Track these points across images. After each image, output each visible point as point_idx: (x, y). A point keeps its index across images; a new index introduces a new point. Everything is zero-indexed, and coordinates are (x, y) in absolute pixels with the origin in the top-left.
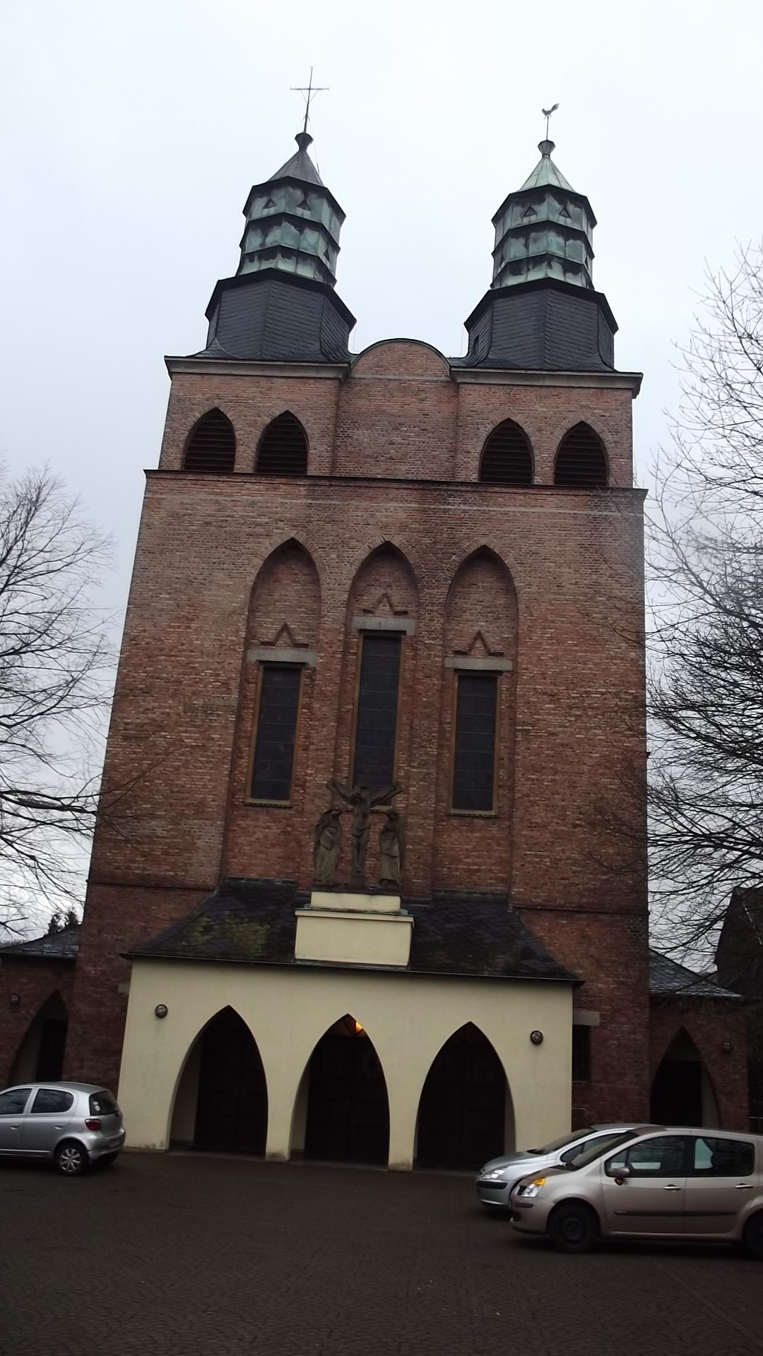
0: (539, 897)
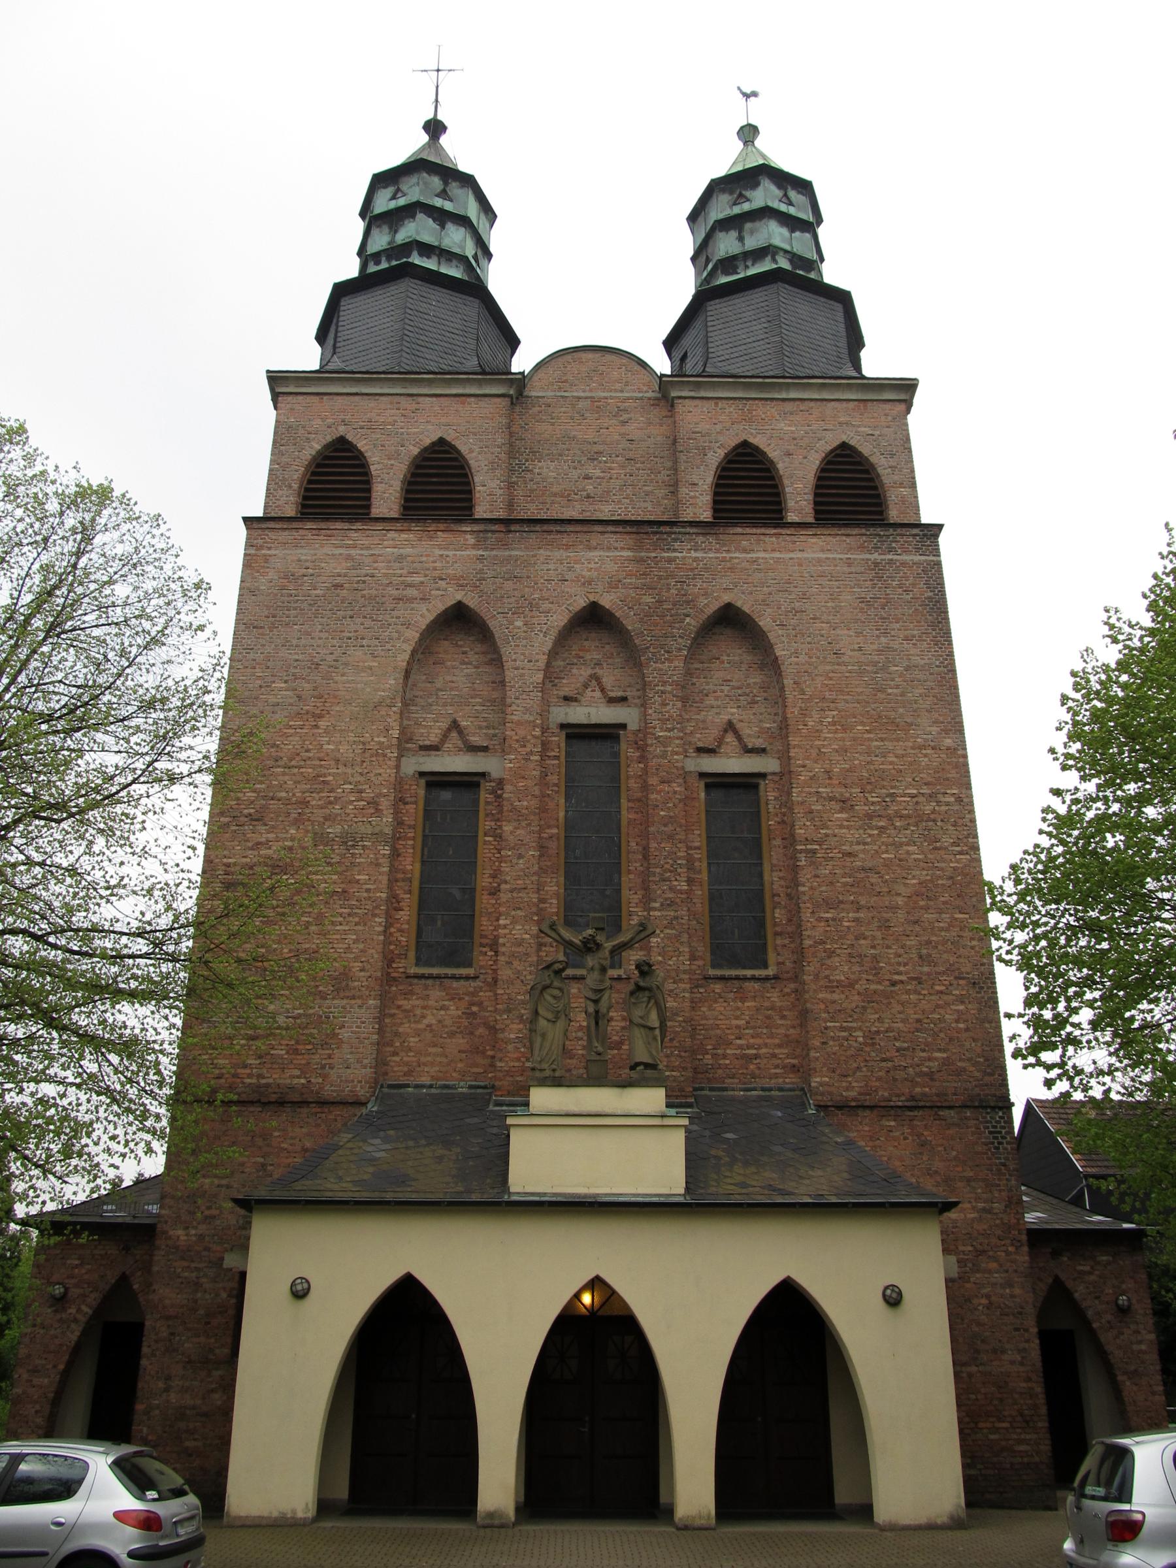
0: (852, 1089)
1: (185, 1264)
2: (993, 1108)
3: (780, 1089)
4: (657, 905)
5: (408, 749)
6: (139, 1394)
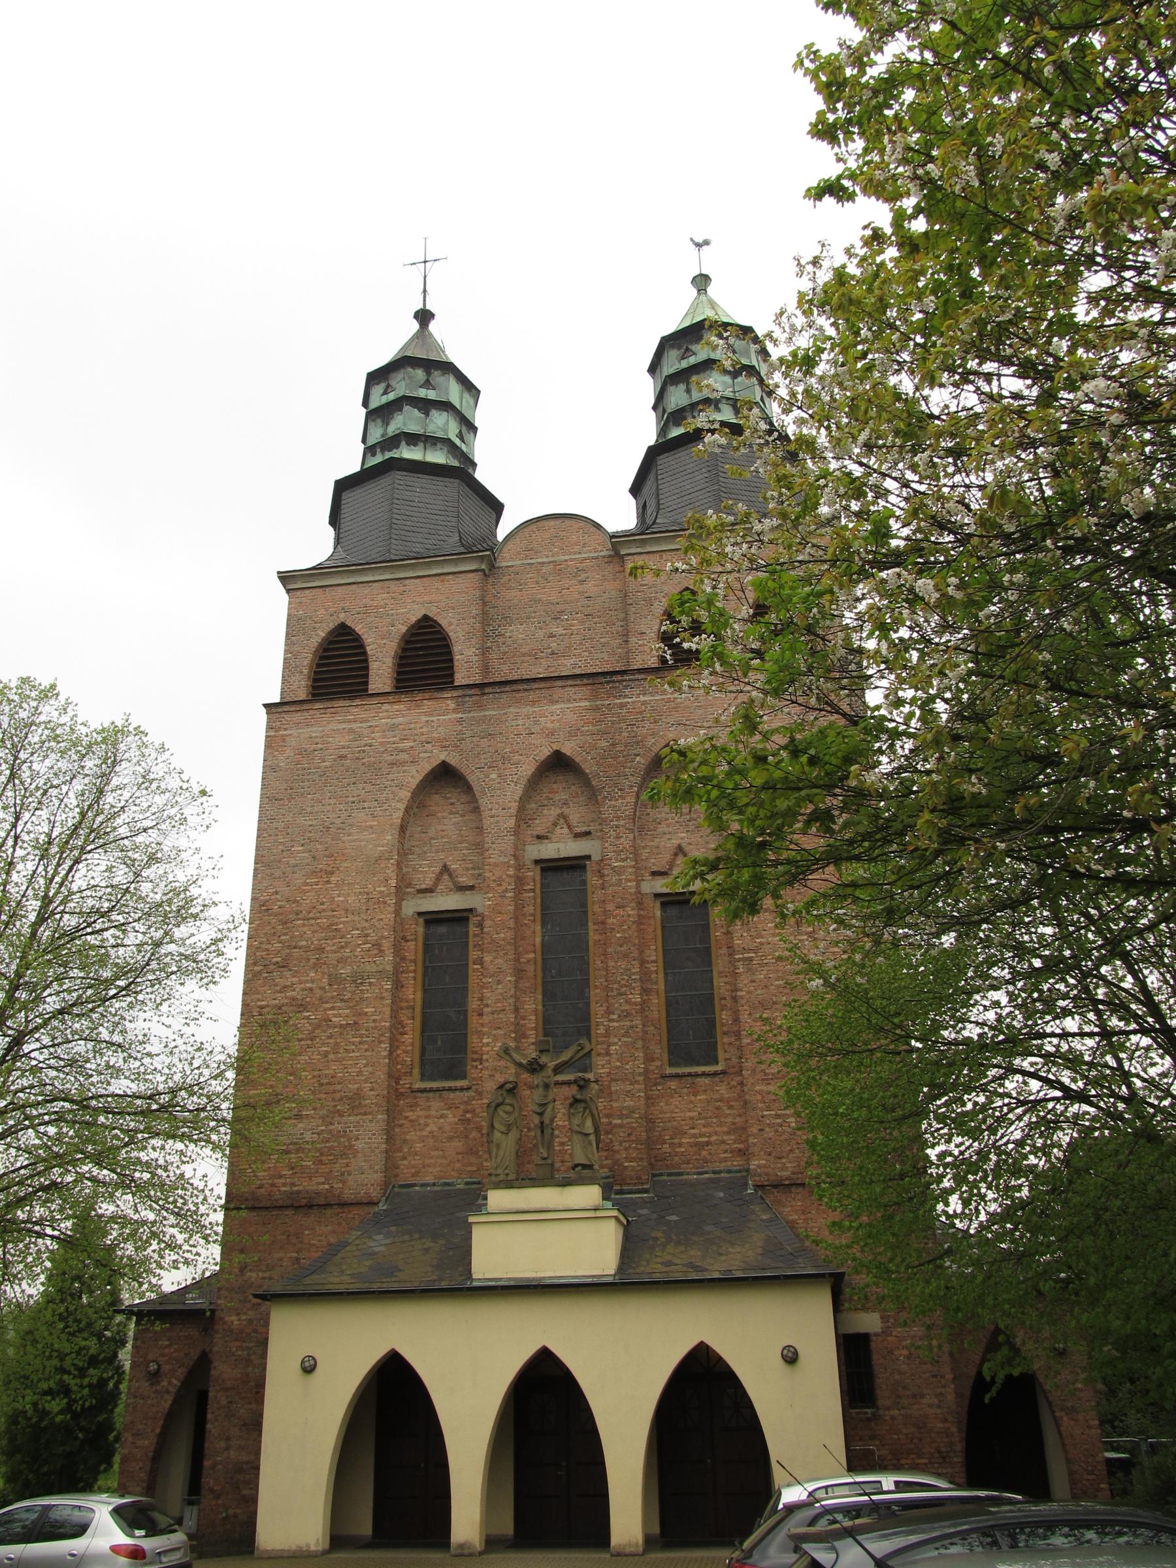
1: (238, 1344)
3: (729, 1171)
4: (615, 1017)
5: (408, 893)
6: (206, 1452)
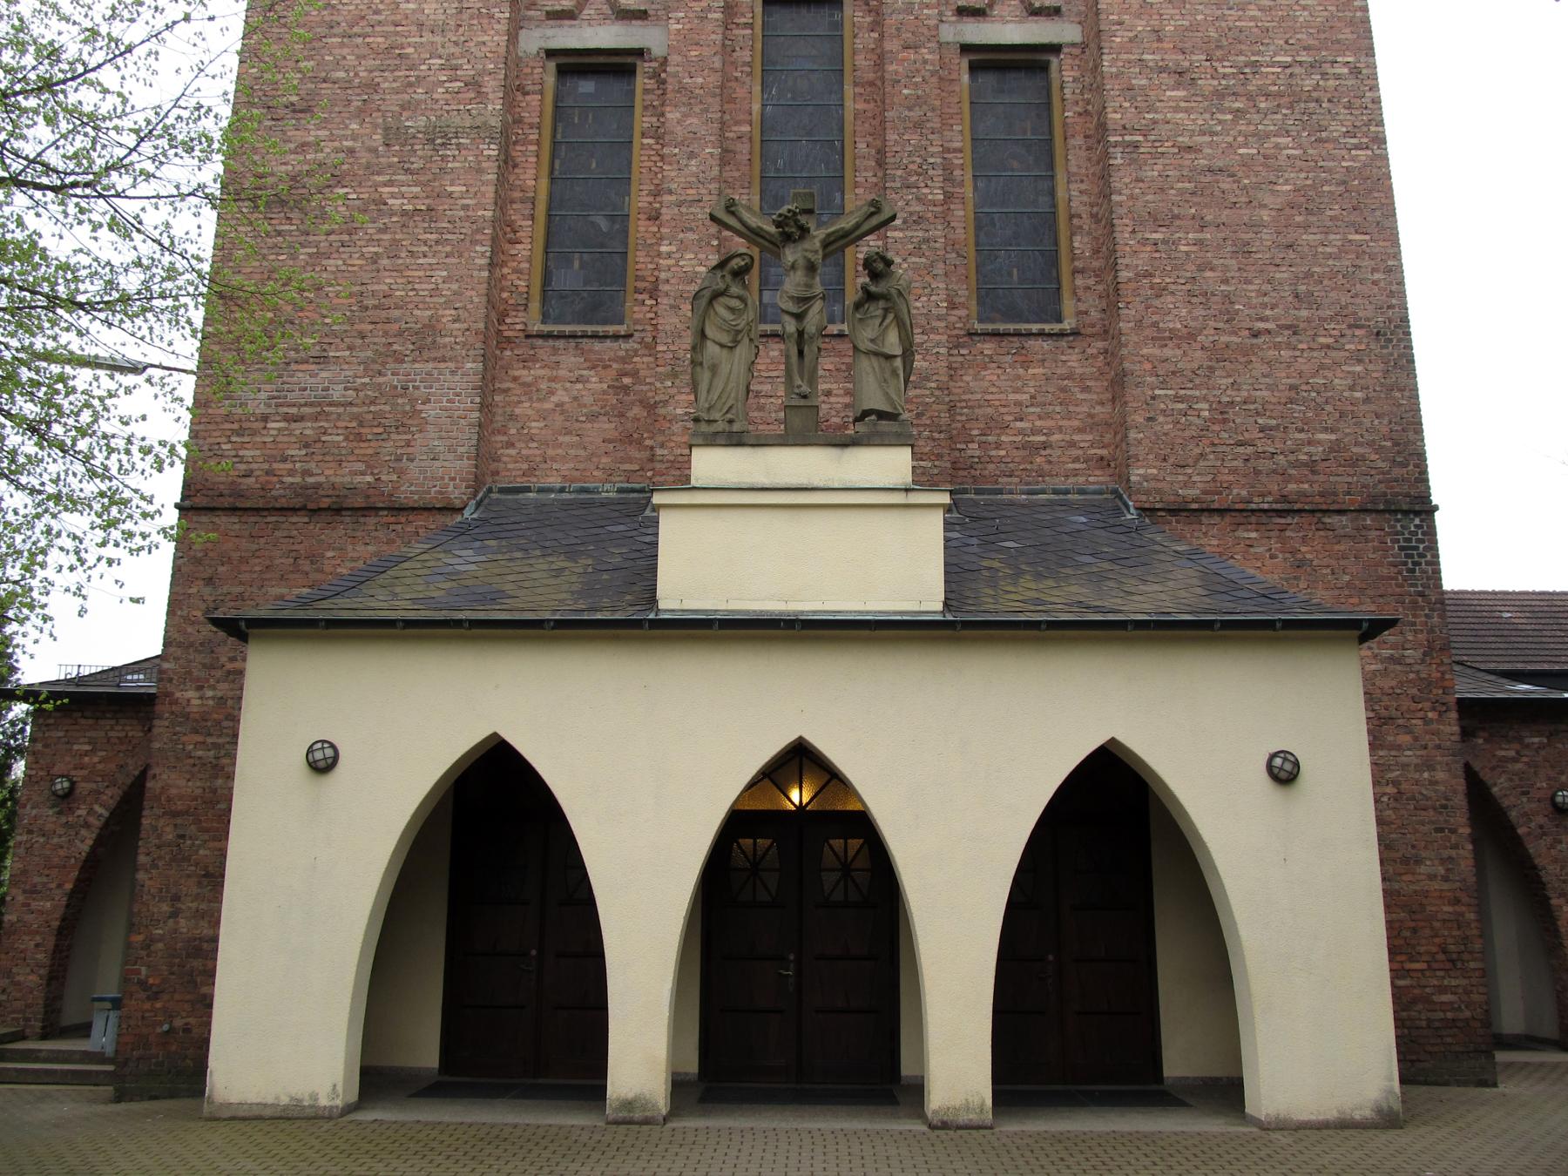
1: (200, 738)
2: (1406, 513)
3: (1082, 492)
5: (530, 19)
